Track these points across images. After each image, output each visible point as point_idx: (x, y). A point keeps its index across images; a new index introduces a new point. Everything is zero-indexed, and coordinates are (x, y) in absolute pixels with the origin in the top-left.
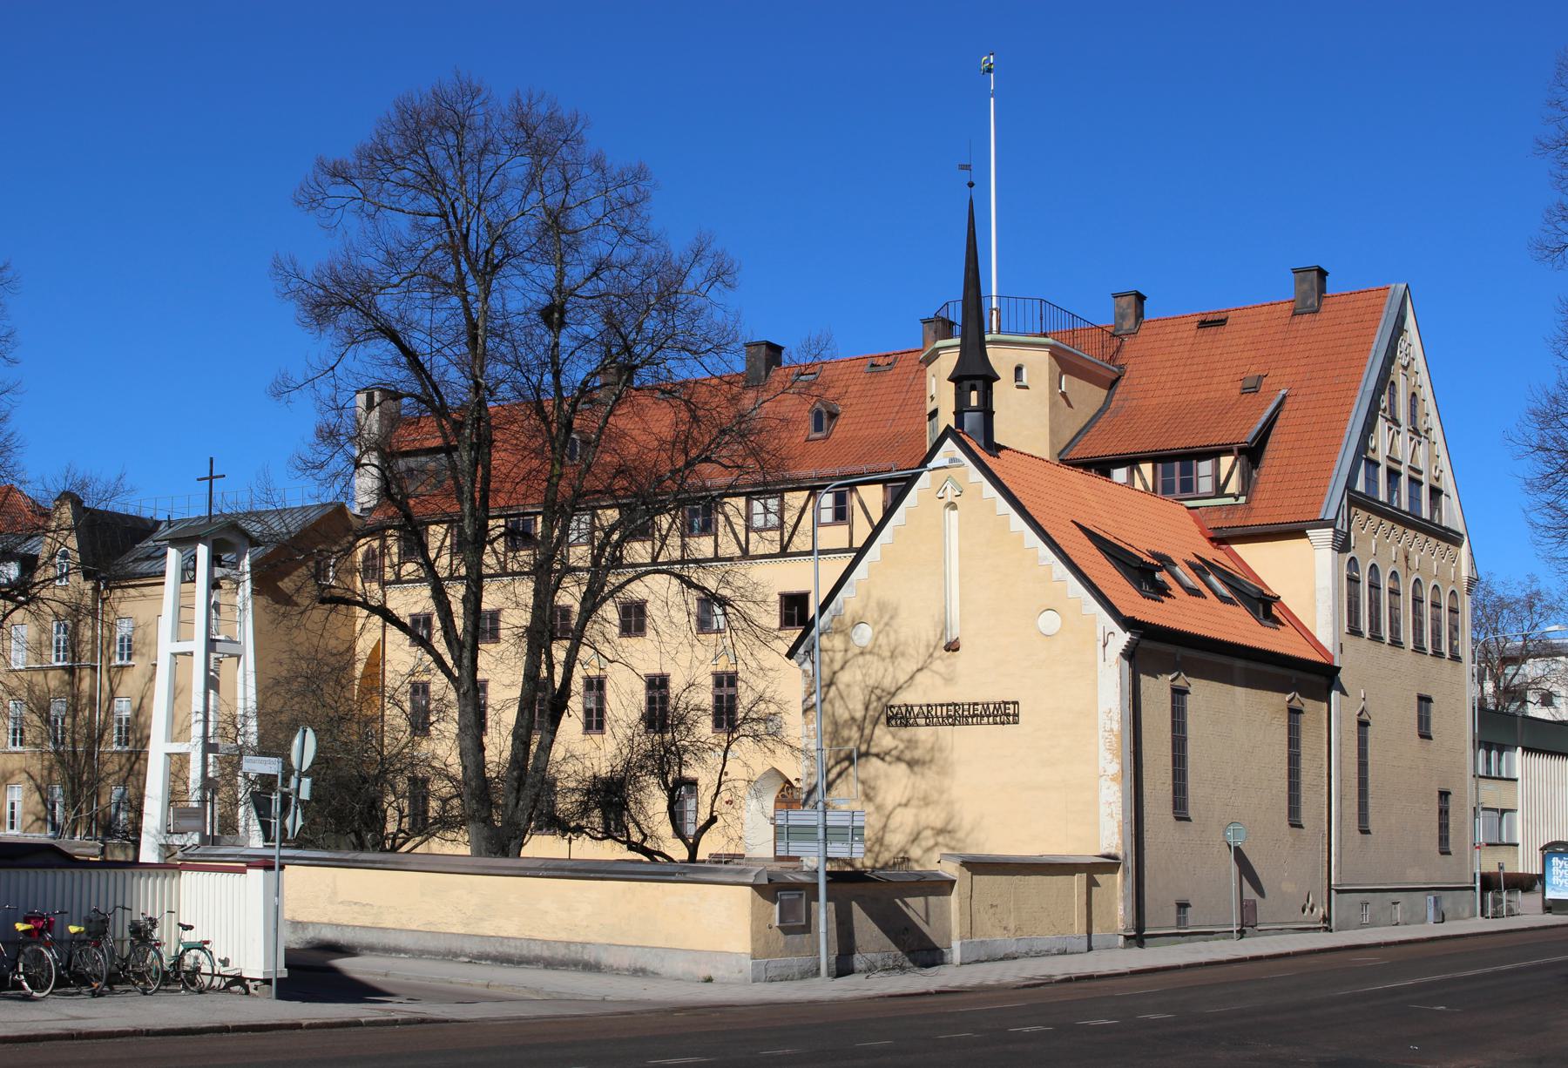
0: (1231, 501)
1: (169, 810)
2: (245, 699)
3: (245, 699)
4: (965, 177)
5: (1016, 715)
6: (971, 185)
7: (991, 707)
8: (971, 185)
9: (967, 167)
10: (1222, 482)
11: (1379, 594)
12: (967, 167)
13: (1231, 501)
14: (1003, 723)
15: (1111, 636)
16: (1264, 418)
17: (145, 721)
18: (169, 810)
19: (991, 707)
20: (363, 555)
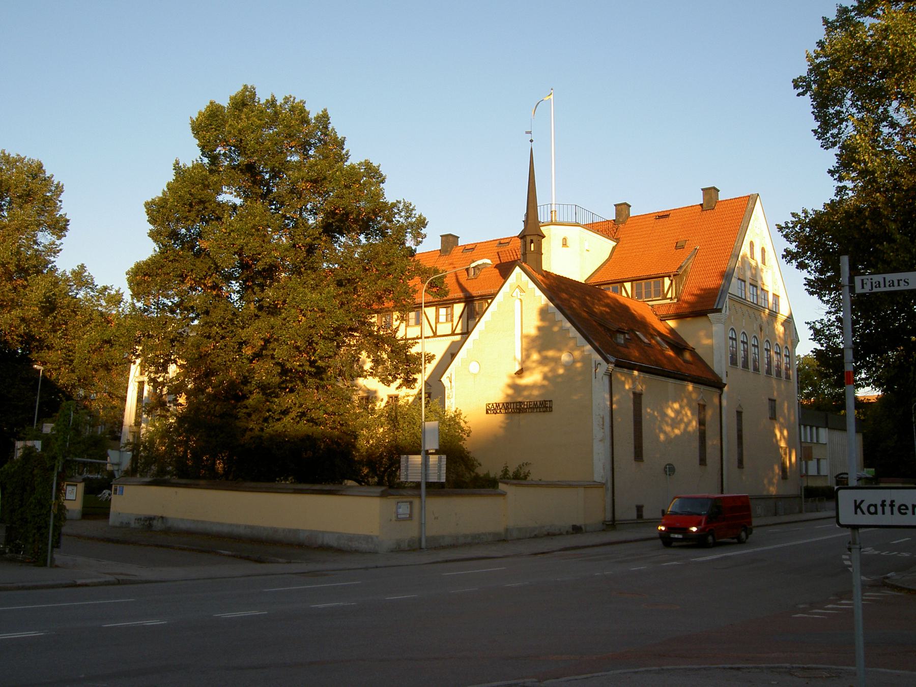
0: (668, 301)
1: (221, 555)
2: (517, 255)
3: (517, 255)
4: (529, 137)
5: (551, 407)
6: (531, 141)
7: (538, 403)
8: (531, 141)
9: (530, 133)
10: (665, 292)
11: (775, 404)
12: (530, 133)
13: (668, 301)
14: (544, 412)
15: (599, 366)
16: (562, 552)
17: (364, 391)
18: (221, 555)
19: (538, 403)
20: (484, 264)
